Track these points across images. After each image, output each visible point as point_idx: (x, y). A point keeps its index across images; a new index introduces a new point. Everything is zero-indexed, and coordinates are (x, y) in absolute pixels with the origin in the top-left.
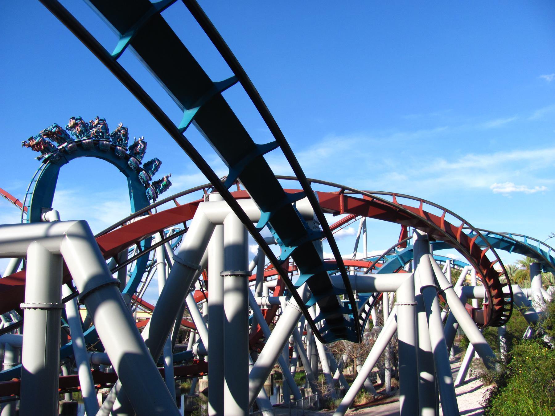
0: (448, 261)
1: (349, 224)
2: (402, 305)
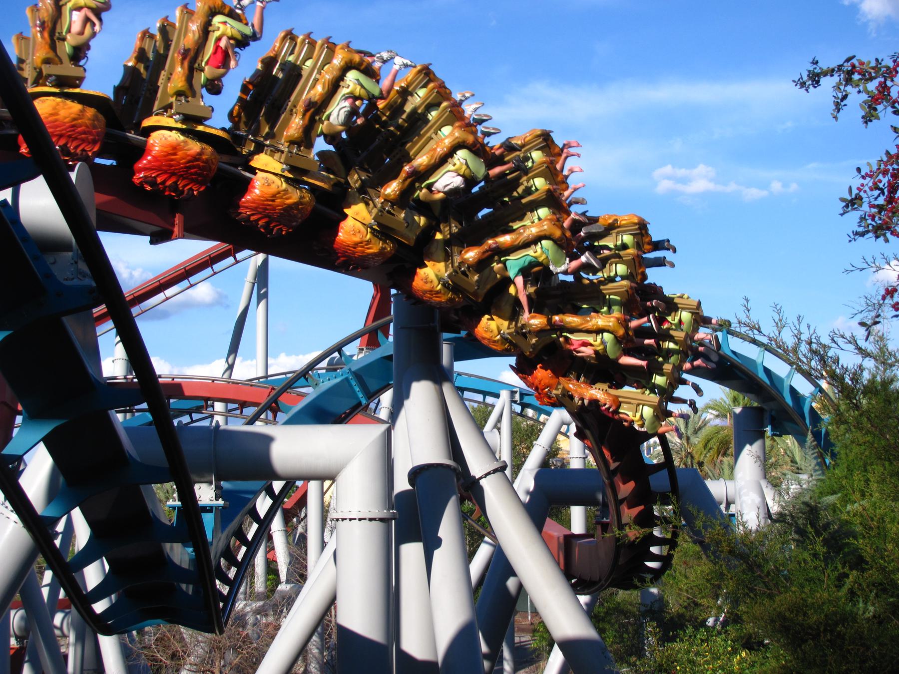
0: (505, 395)
1: (215, 273)
2: (350, 520)
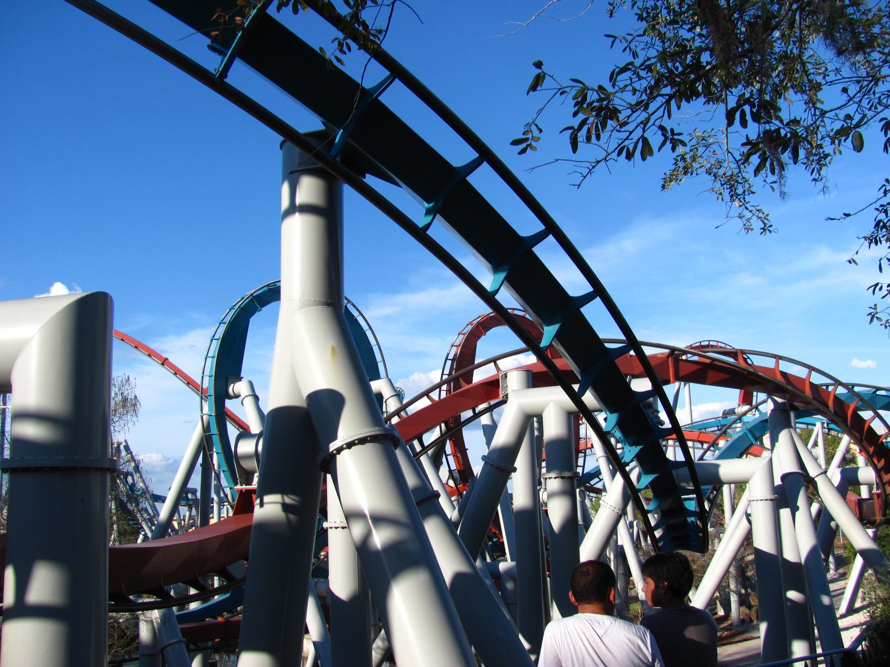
2: (757, 500)
